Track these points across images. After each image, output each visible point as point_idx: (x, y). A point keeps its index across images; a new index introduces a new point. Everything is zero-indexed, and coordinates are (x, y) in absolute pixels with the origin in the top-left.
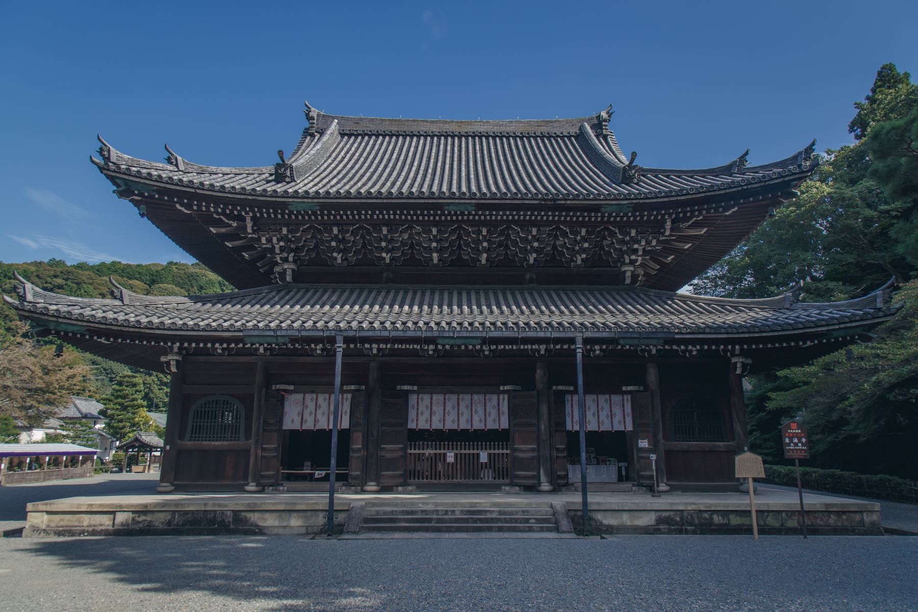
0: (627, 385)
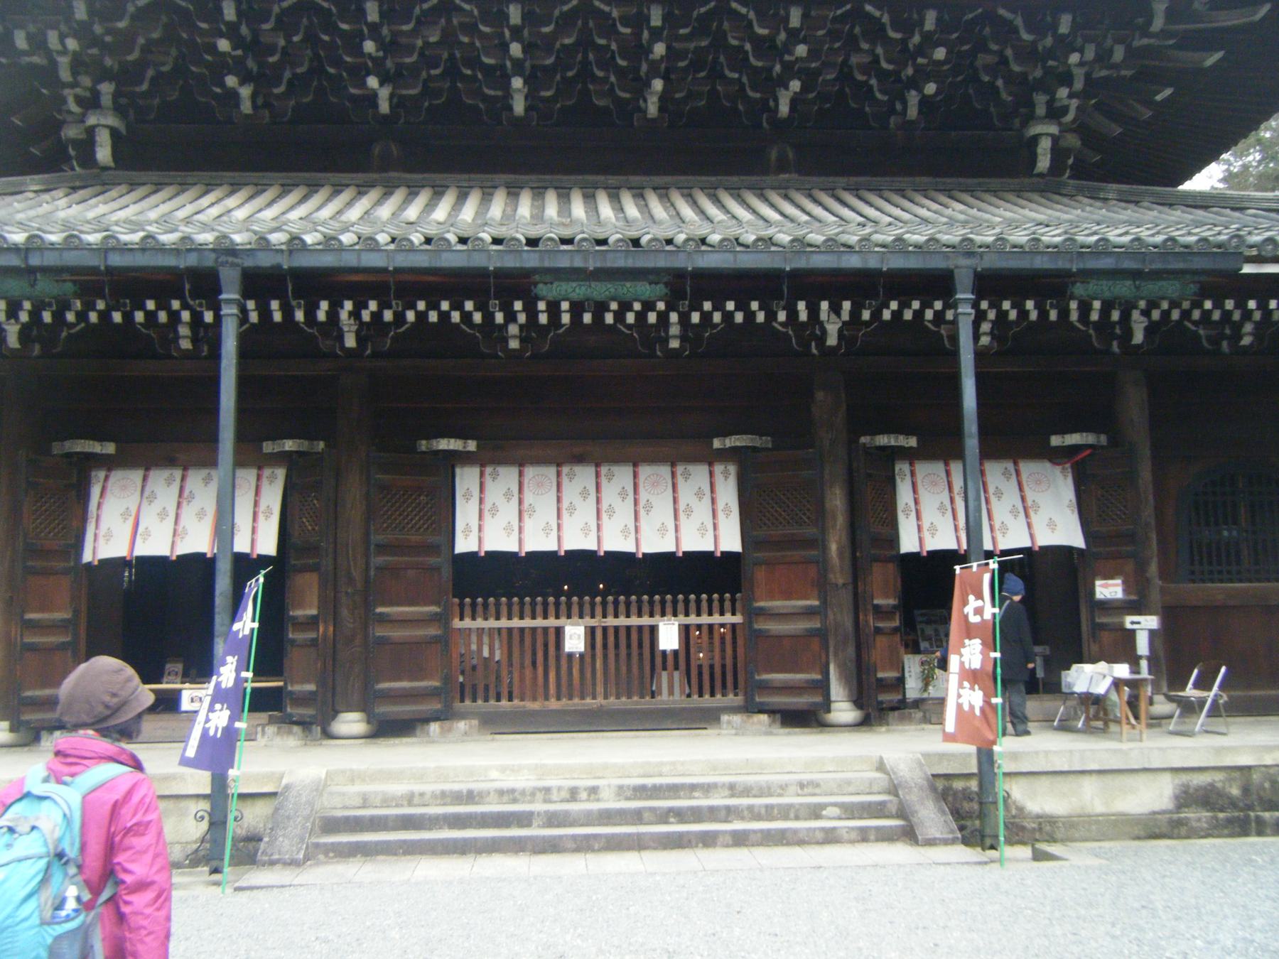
0: (1063, 431)
